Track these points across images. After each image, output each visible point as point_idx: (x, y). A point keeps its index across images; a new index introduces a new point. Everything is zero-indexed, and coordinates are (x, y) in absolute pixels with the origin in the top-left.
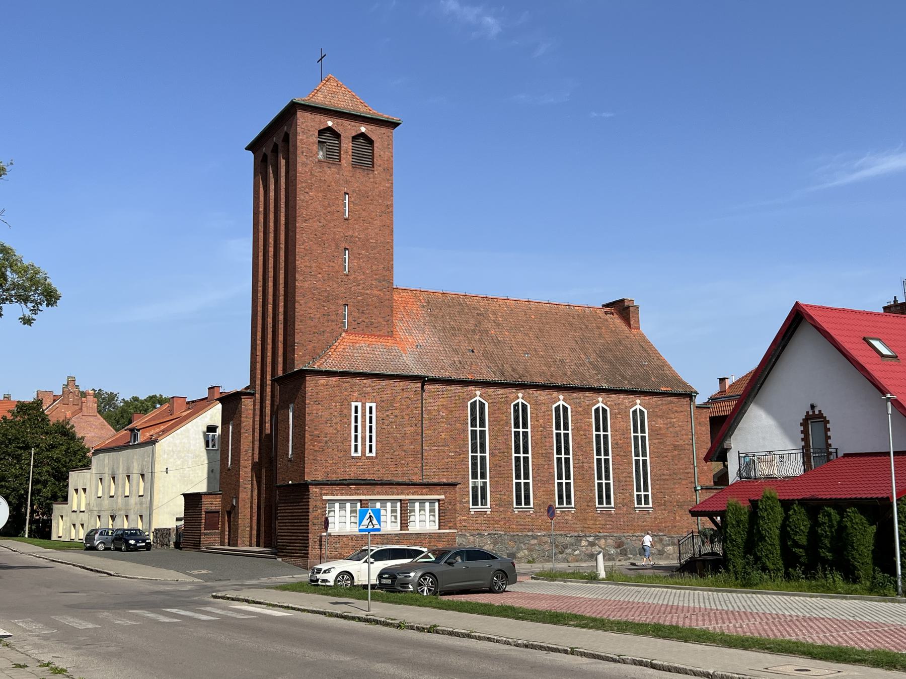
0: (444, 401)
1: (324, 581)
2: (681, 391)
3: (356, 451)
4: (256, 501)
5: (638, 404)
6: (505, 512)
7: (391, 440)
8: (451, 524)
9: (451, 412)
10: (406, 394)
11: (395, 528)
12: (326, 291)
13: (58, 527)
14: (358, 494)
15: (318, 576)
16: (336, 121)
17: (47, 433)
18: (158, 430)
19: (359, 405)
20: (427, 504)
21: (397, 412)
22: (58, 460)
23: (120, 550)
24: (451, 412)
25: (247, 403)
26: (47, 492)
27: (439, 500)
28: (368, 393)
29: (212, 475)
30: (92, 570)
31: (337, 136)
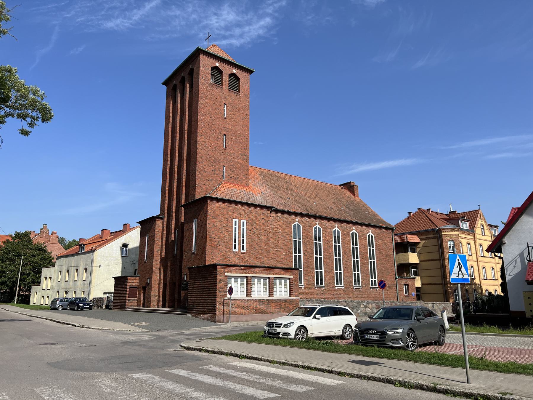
0: (281, 223)
1: (285, 334)
2: (388, 227)
3: (235, 248)
4: (162, 281)
5: (370, 232)
6: (310, 288)
7: (255, 243)
8: (296, 294)
9: (284, 229)
10: (262, 217)
11: (265, 295)
12: (213, 157)
13: (34, 298)
14: (245, 273)
15: (279, 330)
16: (221, 64)
17: (31, 249)
18: (95, 246)
19: (237, 221)
20: (283, 281)
21: (257, 227)
22: (37, 263)
23: (73, 310)
24: (284, 229)
25: (159, 223)
26: (29, 280)
27: (289, 279)
28: (242, 214)
29: (124, 270)
30: (60, 322)
31: (221, 72)
